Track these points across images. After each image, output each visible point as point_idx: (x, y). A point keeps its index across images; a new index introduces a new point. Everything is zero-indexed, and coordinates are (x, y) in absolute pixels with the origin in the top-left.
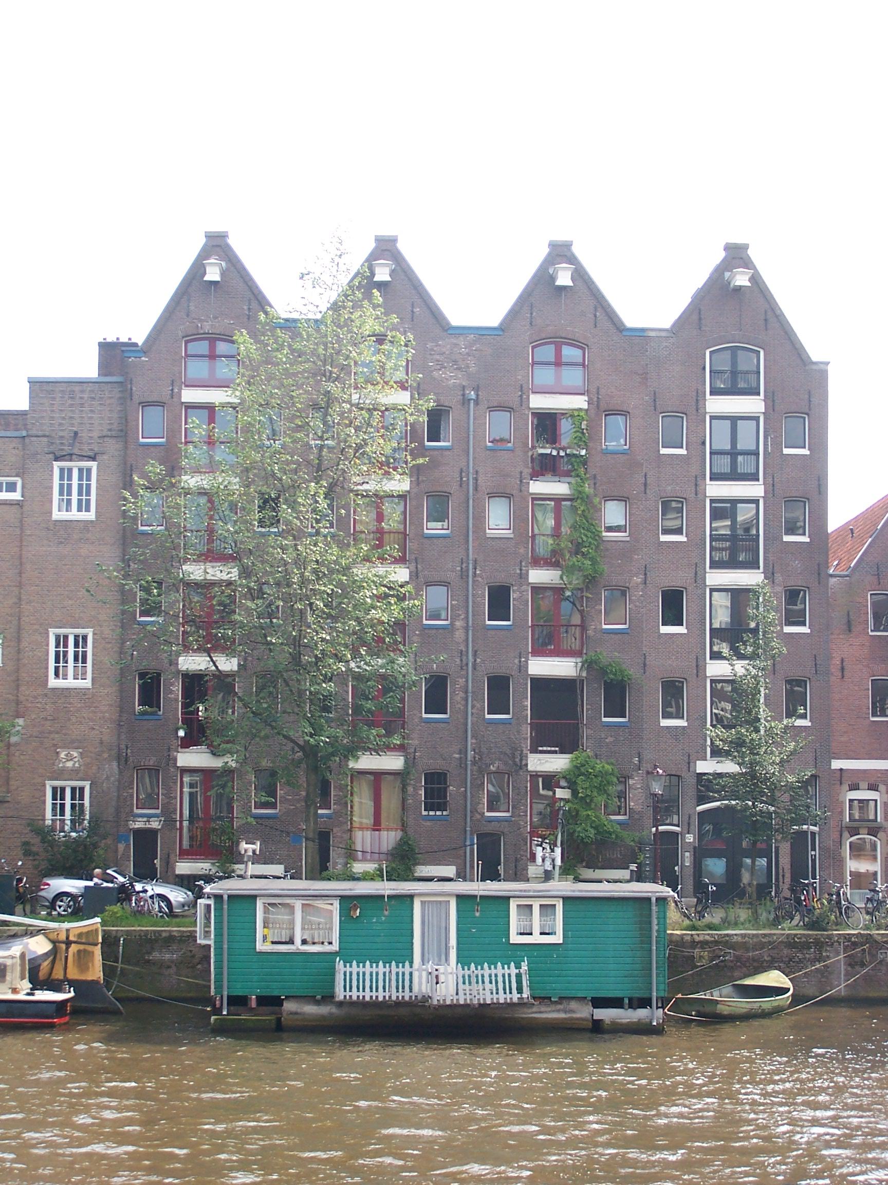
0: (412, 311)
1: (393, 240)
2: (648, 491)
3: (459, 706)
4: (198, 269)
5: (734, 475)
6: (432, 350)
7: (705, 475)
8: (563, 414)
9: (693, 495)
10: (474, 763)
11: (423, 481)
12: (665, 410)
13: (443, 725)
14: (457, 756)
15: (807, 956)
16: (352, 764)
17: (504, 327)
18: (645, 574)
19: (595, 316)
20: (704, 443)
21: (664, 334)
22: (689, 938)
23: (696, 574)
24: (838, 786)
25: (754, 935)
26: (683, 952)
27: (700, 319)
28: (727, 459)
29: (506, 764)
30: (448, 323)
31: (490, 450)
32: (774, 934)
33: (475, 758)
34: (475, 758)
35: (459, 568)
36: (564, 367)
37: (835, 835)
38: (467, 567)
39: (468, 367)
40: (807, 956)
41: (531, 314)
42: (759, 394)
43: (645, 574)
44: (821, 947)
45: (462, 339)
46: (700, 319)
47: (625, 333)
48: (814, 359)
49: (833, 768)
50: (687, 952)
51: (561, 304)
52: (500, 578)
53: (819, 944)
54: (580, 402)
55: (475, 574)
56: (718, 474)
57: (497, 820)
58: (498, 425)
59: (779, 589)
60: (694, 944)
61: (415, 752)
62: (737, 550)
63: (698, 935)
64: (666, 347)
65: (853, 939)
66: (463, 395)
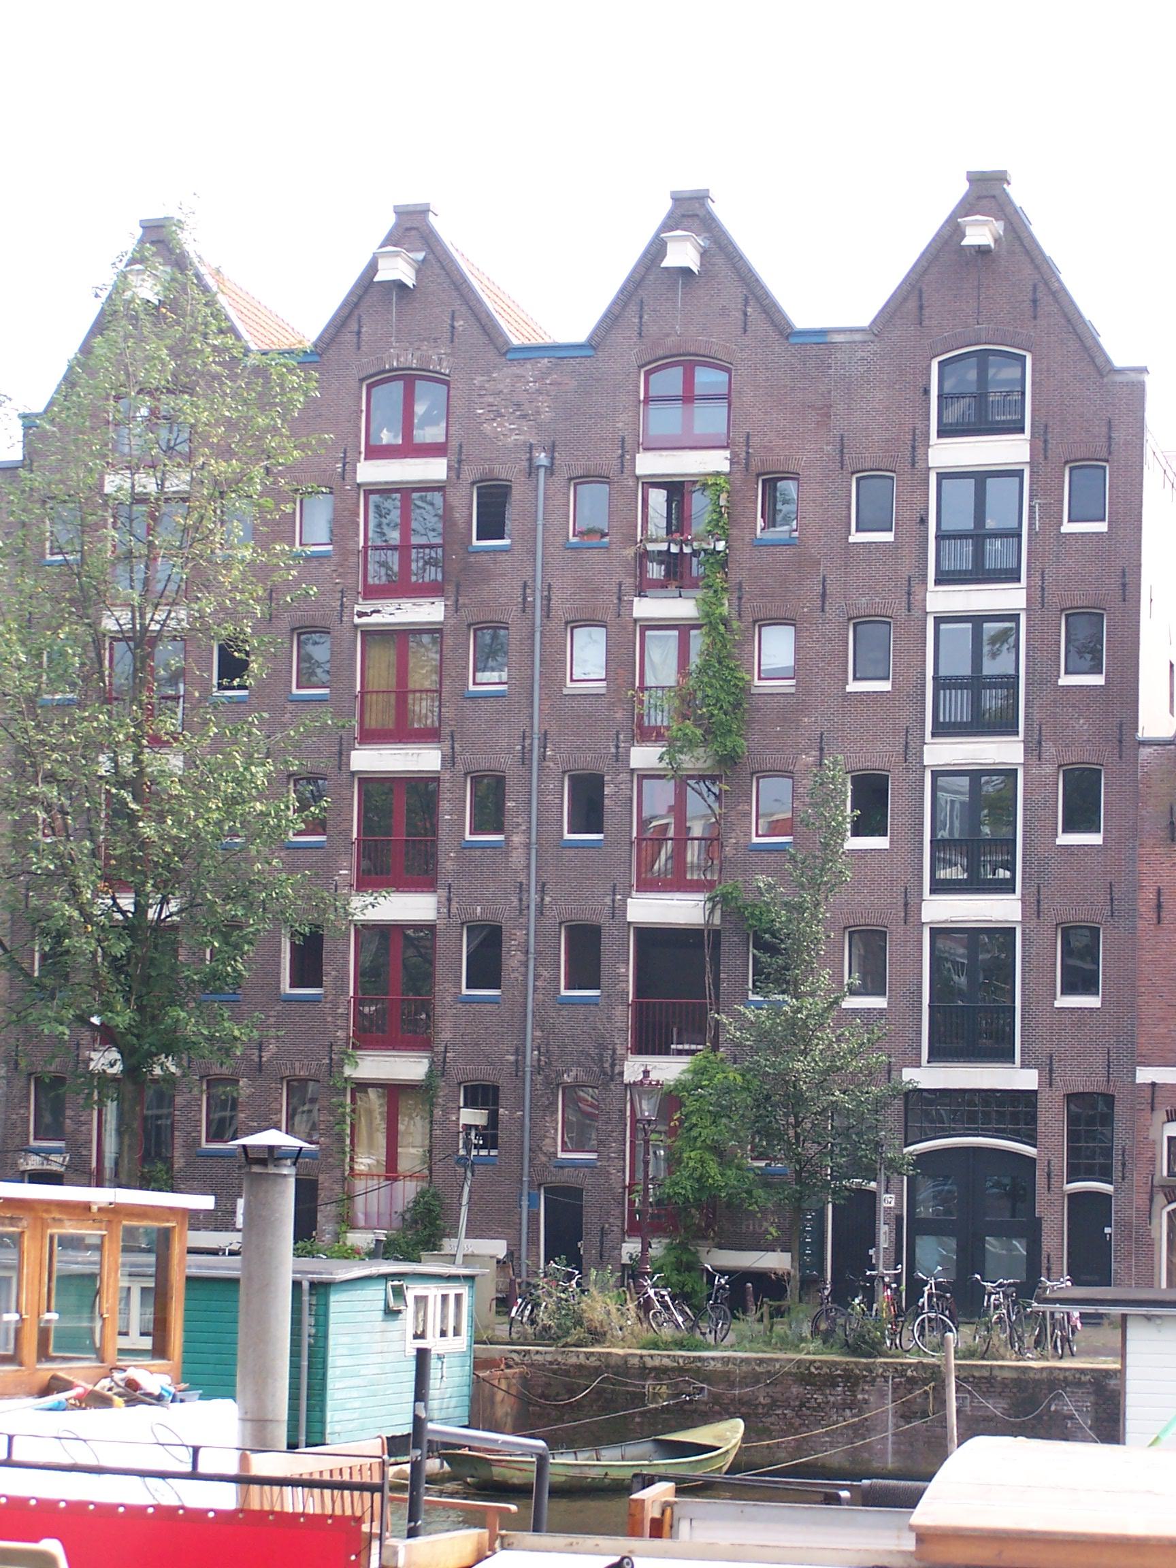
0: (453, 327)
1: (422, 212)
2: (827, 608)
3: (516, 975)
4: (952, 231)
5: (979, 574)
6: (482, 388)
7: (926, 575)
8: (694, 482)
9: (904, 612)
10: (538, 1069)
11: (464, 605)
12: (859, 467)
13: (489, 1007)
14: (512, 1058)
15: (832, 1399)
16: (348, 1071)
17: (594, 344)
18: (821, 749)
19: (745, 314)
20: (923, 521)
21: (858, 337)
22: (636, 1361)
23: (906, 746)
24: (1147, 1114)
25: (743, 1360)
26: (626, 1384)
27: (921, 307)
28: (968, 547)
29: (589, 1072)
30: (788, 324)
31: (574, 548)
32: (777, 1360)
33: (539, 1060)
34: (539, 1060)
35: (519, 748)
36: (697, 404)
37: (1140, 1200)
38: (531, 744)
39: (538, 413)
40: (832, 1399)
41: (641, 317)
42: (1022, 431)
43: (821, 749)
44: (856, 1384)
45: (529, 366)
46: (921, 307)
47: (793, 340)
48: (1118, 361)
49: (1138, 1081)
50: (633, 1385)
51: (413, 314)
52: (586, 762)
53: (851, 1380)
54: (717, 461)
55: (543, 757)
56: (948, 572)
57: (574, 1164)
58: (591, 506)
59: (1049, 769)
60: (644, 1371)
61: (446, 1052)
62: (982, 705)
63: (651, 1356)
64: (863, 359)
65: (909, 1373)
66: (530, 460)
